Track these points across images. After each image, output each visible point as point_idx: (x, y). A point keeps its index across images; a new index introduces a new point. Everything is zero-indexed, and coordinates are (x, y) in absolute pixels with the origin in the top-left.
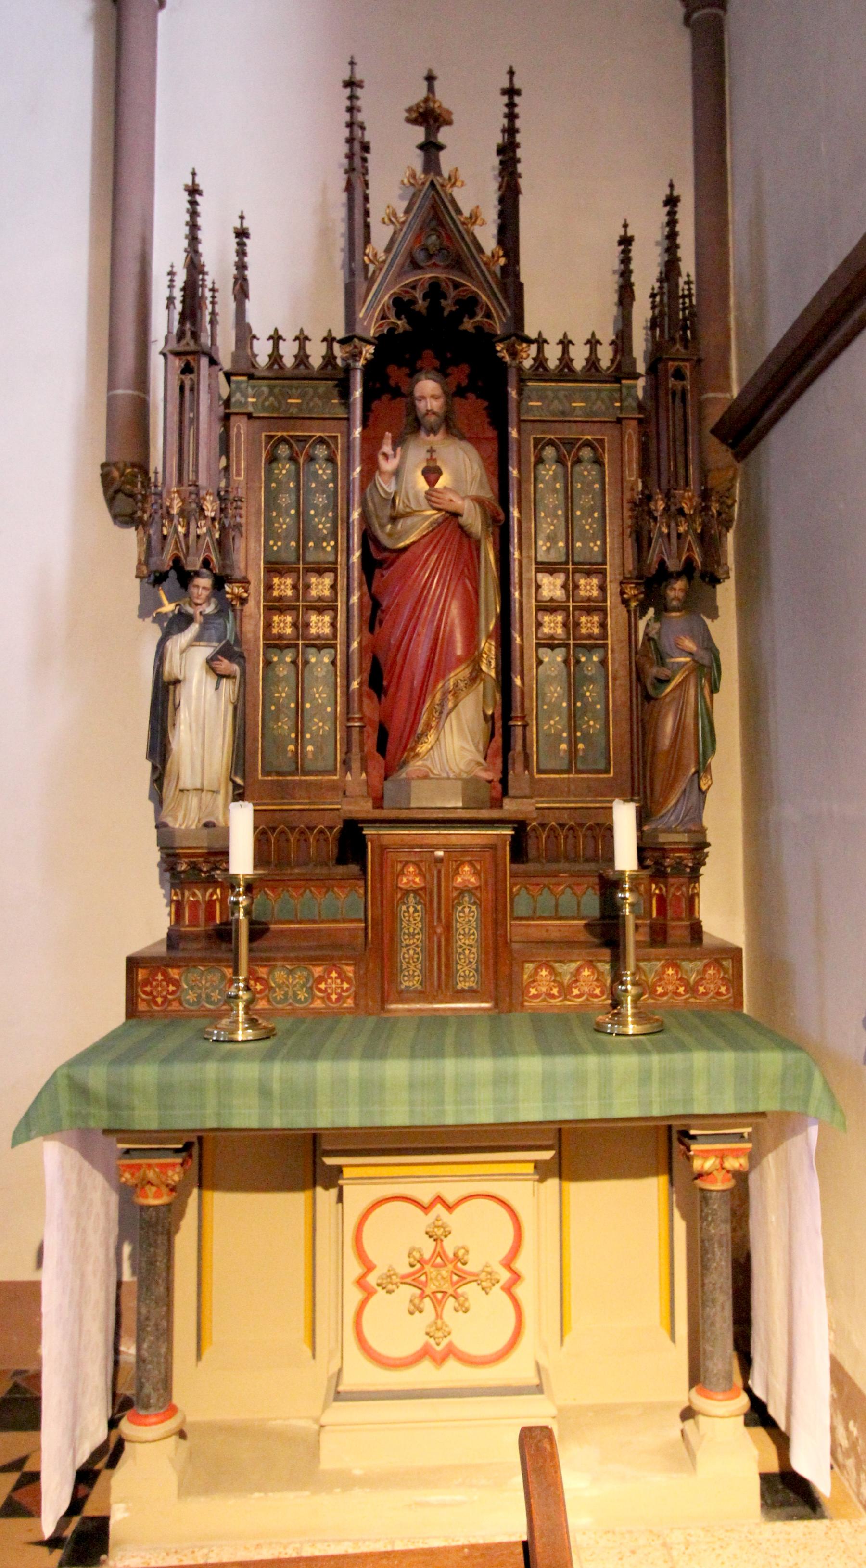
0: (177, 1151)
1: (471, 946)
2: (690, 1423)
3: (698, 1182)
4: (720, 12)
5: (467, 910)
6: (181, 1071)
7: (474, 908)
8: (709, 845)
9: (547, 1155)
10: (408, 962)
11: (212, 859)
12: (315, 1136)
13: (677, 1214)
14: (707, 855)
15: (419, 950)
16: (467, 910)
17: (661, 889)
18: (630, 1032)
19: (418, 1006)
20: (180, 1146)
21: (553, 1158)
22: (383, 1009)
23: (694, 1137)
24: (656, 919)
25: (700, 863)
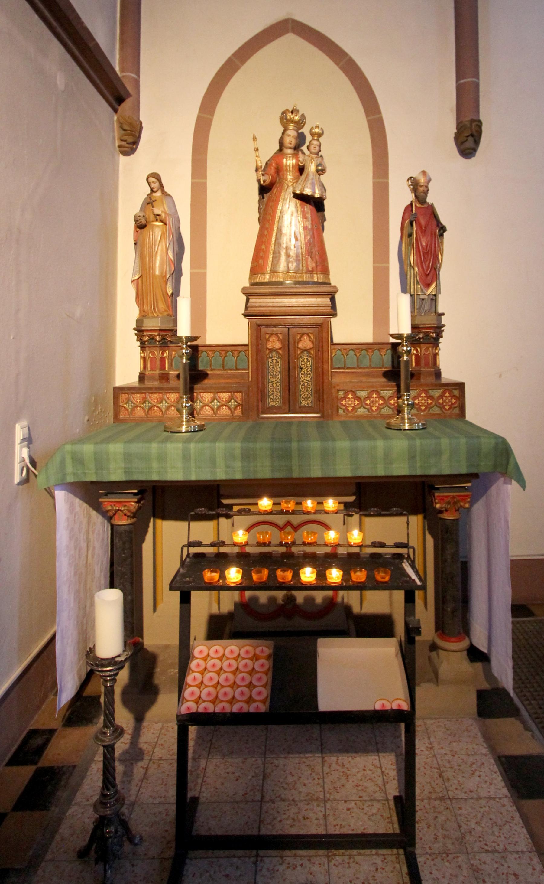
0: (135, 494)
1: (308, 381)
2: (434, 654)
3: (441, 516)
4: (378, 116)
5: (305, 360)
6: (137, 448)
7: (310, 359)
8: (444, 326)
9: (351, 499)
10: (273, 391)
11: (162, 333)
12: (218, 486)
13: (427, 532)
14: (443, 330)
15: (278, 384)
16: (305, 360)
17: (417, 351)
18: (407, 428)
19: (266, 291)
20: (136, 491)
21: (354, 501)
22: (258, 416)
23: (438, 489)
24: (414, 368)
25: (439, 335)
